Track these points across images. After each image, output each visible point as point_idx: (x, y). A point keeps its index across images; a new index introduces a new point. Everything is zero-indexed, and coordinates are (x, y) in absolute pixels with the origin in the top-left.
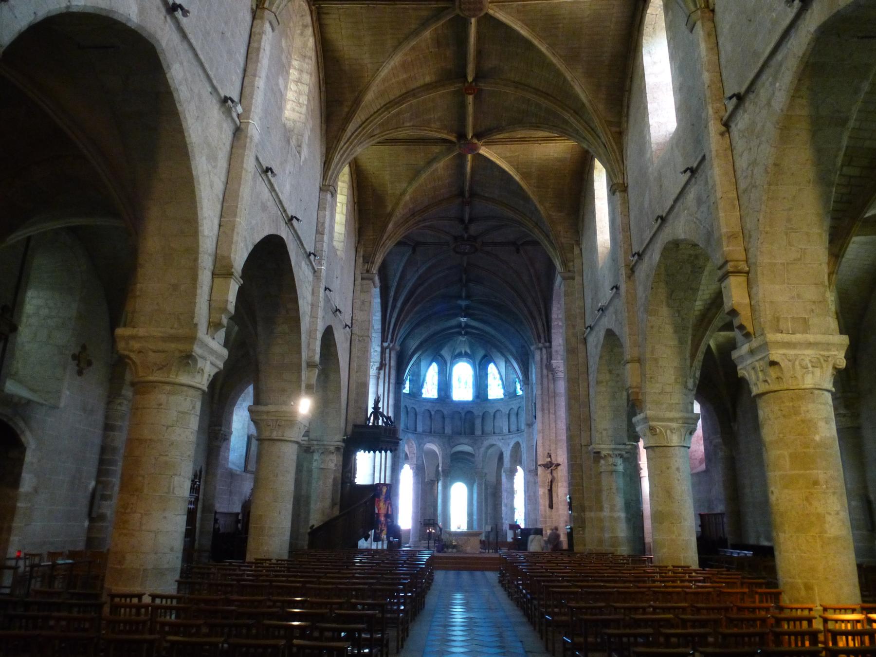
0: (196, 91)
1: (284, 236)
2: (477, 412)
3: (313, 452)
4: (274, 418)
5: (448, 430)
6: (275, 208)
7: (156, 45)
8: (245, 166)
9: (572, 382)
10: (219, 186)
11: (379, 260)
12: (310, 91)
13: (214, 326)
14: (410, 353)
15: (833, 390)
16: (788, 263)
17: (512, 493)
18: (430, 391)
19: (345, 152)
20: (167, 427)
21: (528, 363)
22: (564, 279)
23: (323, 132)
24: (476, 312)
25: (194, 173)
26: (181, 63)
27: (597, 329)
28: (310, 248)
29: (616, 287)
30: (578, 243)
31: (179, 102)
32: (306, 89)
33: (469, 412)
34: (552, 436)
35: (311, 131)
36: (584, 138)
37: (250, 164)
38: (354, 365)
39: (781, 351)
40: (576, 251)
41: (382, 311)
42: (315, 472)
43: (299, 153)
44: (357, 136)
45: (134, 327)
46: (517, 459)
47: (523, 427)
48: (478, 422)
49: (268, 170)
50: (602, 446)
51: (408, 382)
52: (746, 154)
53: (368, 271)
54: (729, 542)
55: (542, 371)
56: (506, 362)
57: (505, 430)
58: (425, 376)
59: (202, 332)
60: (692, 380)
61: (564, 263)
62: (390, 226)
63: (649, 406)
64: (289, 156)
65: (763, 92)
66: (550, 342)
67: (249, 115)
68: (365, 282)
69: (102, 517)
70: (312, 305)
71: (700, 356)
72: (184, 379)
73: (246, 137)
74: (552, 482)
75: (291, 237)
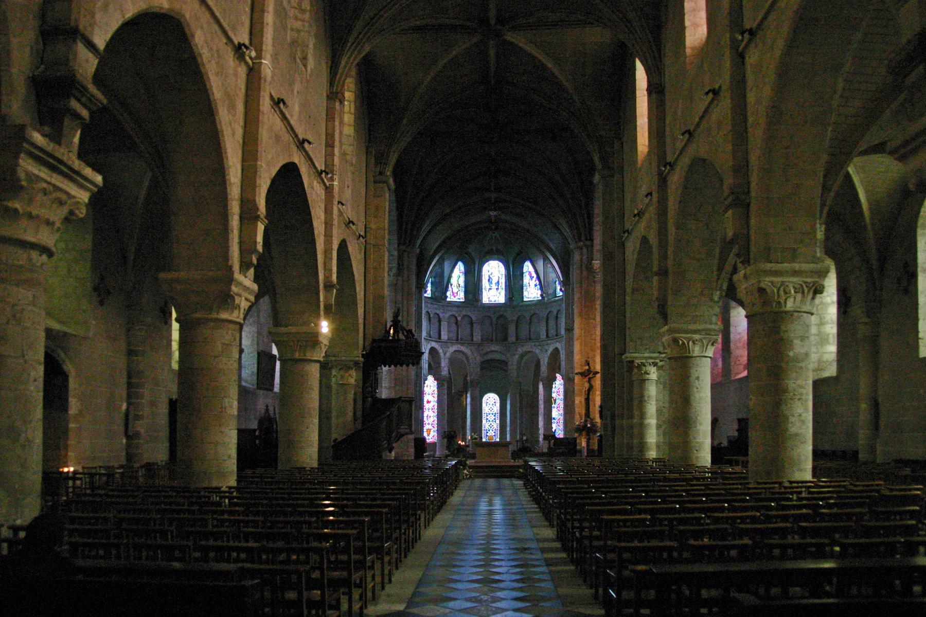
0: (215, 48)
1: (296, 161)
2: (511, 316)
5: (477, 337)
6: (287, 135)
7: (182, 20)
8: (261, 108)
9: (608, 289)
11: (393, 159)
13: (245, 266)
17: (549, 401)
18: (456, 292)
22: (603, 177)
25: (219, 127)
34: (586, 345)
35: (316, 37)
37: (265, 104)
38: (371, 277)
39: (768, 279)
40: (617, 146)
42: (334, 386)
43: (305, 66)
46: (555, 367)
48: (512, 329)
51: (429, 285)
52: (754, 89)
55: (582, 273)
57: (543, 337)
59: (238, 276)
60: (718, 292)
61: (603, 159)
66: (592, 240)
69: (137, 435)
70: (326, 223)
72: (224, 316)
73: (260, 78)
75: (303, 159)
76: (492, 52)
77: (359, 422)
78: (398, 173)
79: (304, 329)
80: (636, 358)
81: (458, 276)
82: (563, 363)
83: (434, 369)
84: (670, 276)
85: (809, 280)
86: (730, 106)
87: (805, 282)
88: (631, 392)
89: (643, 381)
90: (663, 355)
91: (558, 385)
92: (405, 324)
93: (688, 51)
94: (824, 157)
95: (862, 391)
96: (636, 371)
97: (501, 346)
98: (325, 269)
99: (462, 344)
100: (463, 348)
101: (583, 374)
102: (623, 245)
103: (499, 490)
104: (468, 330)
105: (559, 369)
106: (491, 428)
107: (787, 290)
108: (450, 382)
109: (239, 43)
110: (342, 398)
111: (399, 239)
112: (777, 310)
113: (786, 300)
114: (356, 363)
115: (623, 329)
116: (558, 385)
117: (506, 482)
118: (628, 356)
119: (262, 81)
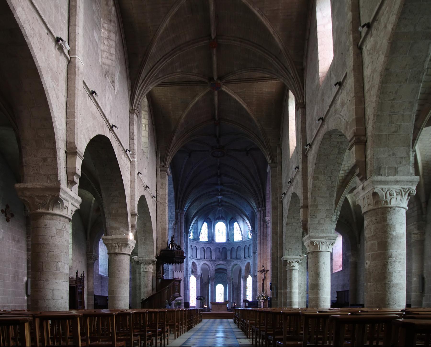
2: (228, 248)
3: (141, 264)
4: (116, 242)
5: (213, 257)
6: (101, 119)
10: (63, 99)
11: (169, 160)
12: (116, 45)
13: (71, 183)
14: (192, 217)
15: (407, 208)
16: (389, 134)
17: (245, 287)
18: (204, 237)
19: (142, 88)
20: (52, 237)
21: (254, 221)
22: (272, 168)
23: (128, 75)
24: (226, 193)
26: (23, 8)
27: (288, 194)
28: (127, 147)
29: (298, 167)
30: (280, 146)
31: (26, 36)
32: (113, 43)
33: (224, 248)
36: (282, 76)
37: (79, 85)
39: (380, 187)
40: (278, 151)
41: (175, 192)
44: (149, 77)
45: (25, 183)
46: (248, 271)
47: (252, 254)
48: (229, 253)
49: (93, 93)
50: (288, 257)
53: (163, 166)
54: (350, 303)
56: (243, 221)
58: (201, 229)
59: (63, 185)
61: (272, 159)
62: (174, 138)
63: (311, 231)
64: (107, 87)
65: (383, 19)
66: (265, 207)
67: (75, 52)
68: (163, 172)
70: (131, 181)
71: (341, 203)
73: (75, 67)
74: (264, 279)
76: (216, 99)
77: (155, 290)
78: (173, 166)
79: (120, 237)
80: (289, 258)
81: (204, 228)
82: (252, 269)
83: (194, 272)
84: (309, 208)
85: (405, 187)
86: (353, 81)
87: (403, 189)
88: (286, 276)
89: (291, 270)
90: (302, 257)
91: (250, 280)
92: (177, 243)
93: (321, 75)
94: (416, 107)
95: (413, 271)
96: (288, 265)
97: (224, 262)
98: (131, 206)
99: (207, 261)
100: (207, 263)
101: (262, 271)
102: (282, 202)
103: (221, 323)
104: (210, 254)
105: (250, 273)
106: (220, 298)
107: (392, 193)
108: (201, 278)
109: (57, 38)
110: (146, 279)
111: (176, 206)
112: (385, 206)
113: (391, 200)
114: (153, 261)
115: (282, 244)
116: (250, 280)
117: (225, 320)
118: (285, 257)
119: (77, 69)
